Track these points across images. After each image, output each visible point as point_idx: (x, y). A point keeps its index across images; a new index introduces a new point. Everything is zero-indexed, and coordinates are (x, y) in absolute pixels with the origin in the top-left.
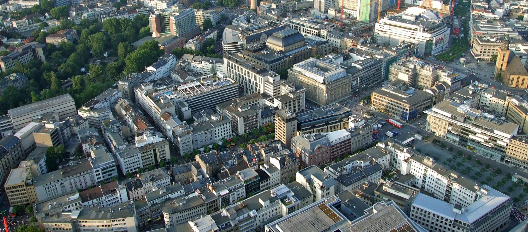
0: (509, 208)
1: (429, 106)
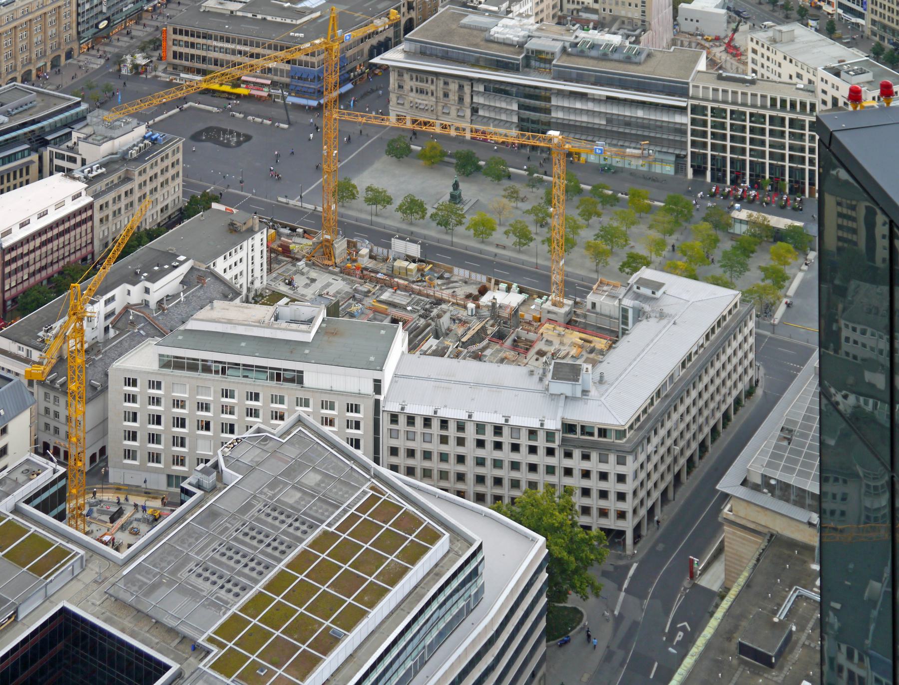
0: (746, 331)
1: (388, 39)
